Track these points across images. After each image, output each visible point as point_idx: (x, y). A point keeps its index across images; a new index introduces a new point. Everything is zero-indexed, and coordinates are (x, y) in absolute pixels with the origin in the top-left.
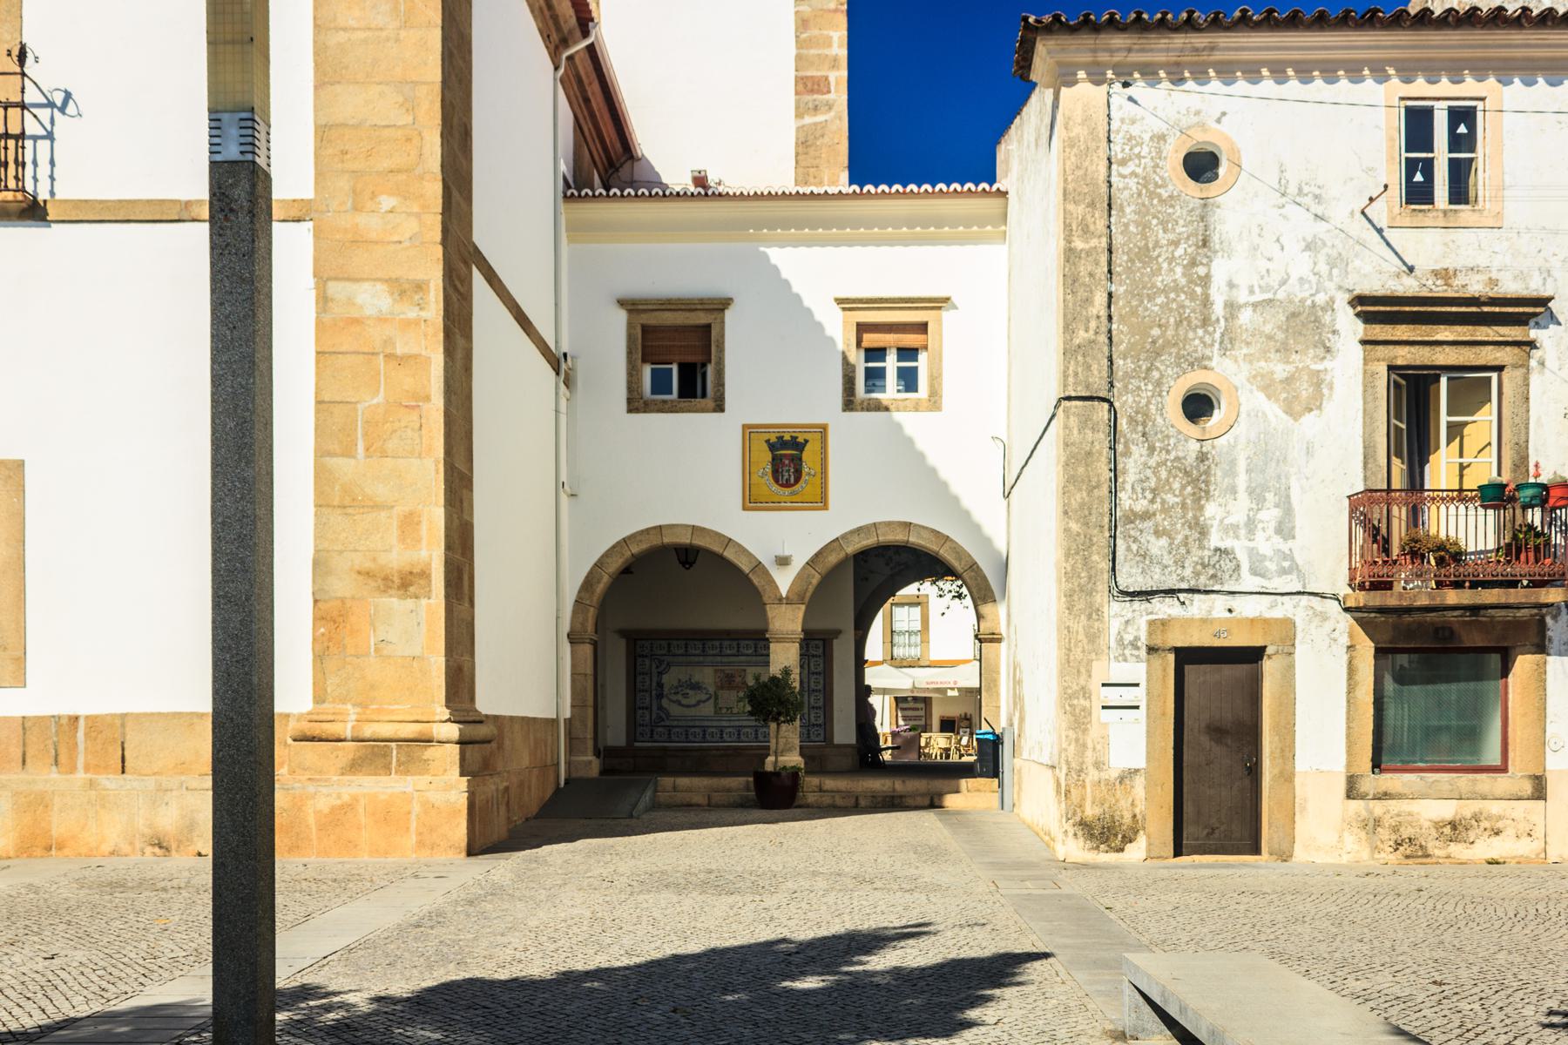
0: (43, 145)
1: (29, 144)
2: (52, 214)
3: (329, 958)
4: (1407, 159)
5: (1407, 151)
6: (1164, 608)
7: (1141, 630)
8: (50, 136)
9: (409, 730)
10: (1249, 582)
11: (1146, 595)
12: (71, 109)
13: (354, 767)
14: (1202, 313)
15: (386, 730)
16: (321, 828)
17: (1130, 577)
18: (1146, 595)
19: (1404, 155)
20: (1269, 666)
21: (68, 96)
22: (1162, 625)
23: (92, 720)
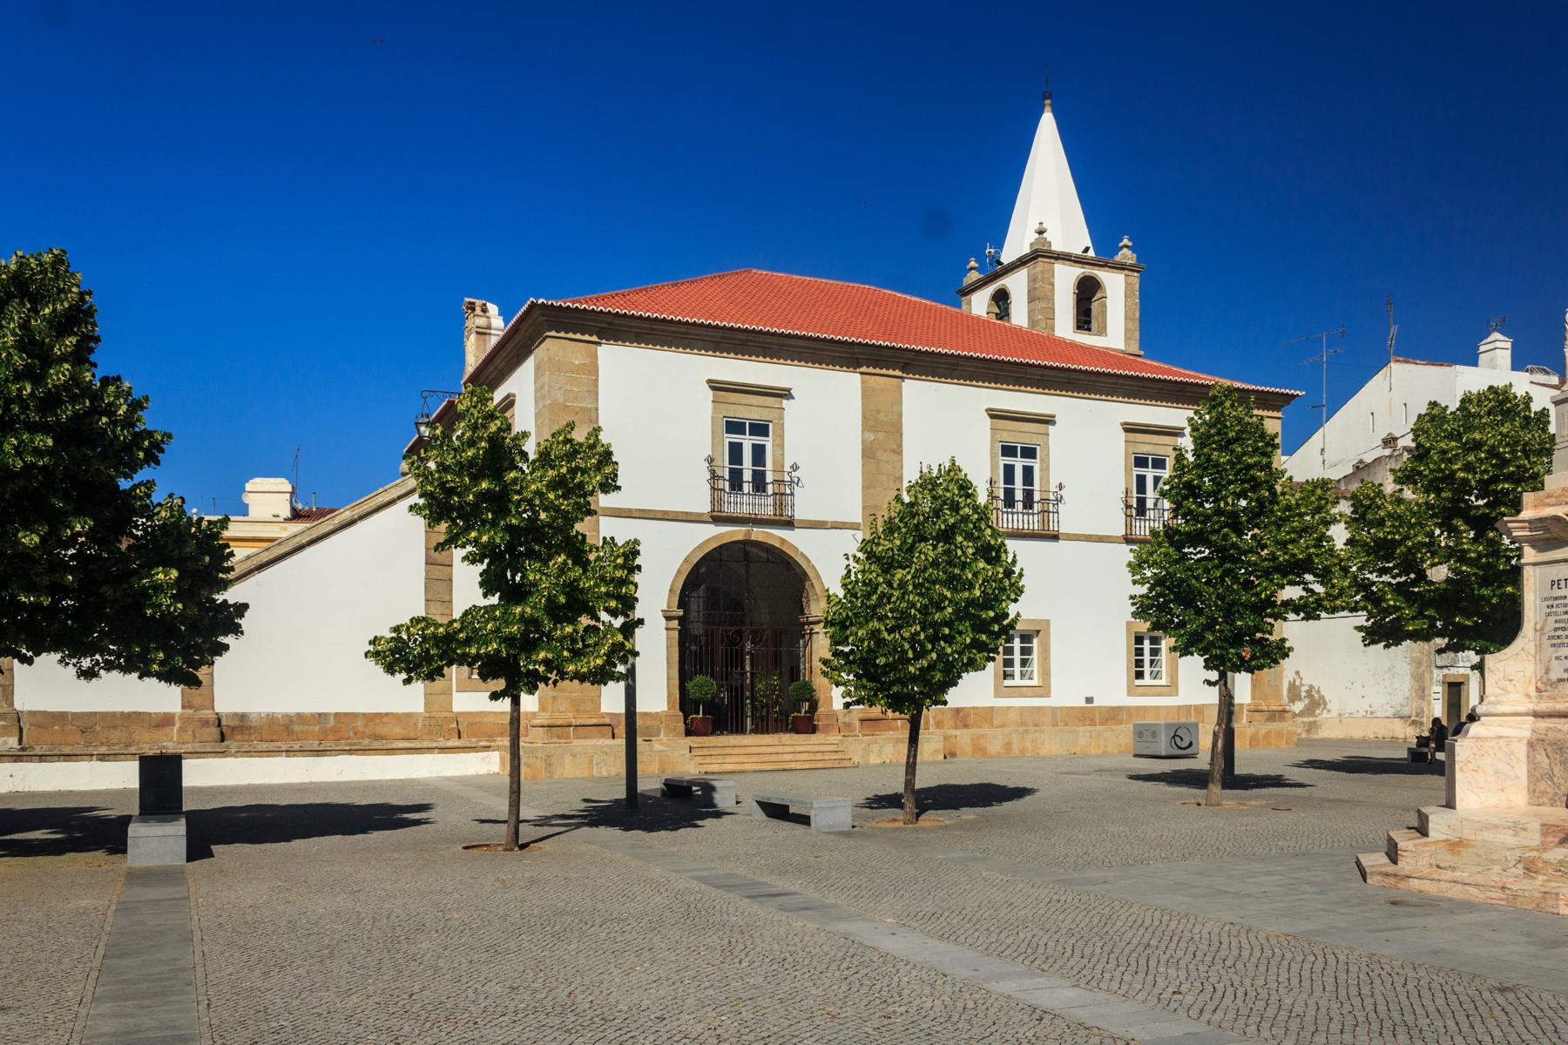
0: (1056, 515)
1: (1051, 515)
2: (796, 525)
3: (348, 748)
4: (750, 435)
5: (745, 434)
6: (1445, 671)
7: (1441, 678)
8: (792, 494)
9: (1280, 708)
10: (1461, 664)
11: (1441, 667)
12: (800, 484)
13: (1268, 720)
14: (1004, 533)
15: (1275, 708)
16: (1264, 739)
17: (1439, 664)
18: (1441, 667)
19: (1019, 458)
20: (1464, 688)
21: (799, 479)
22: (1445, 676)
23: (1195, 706)
